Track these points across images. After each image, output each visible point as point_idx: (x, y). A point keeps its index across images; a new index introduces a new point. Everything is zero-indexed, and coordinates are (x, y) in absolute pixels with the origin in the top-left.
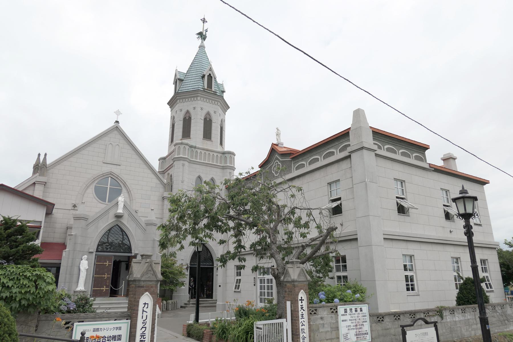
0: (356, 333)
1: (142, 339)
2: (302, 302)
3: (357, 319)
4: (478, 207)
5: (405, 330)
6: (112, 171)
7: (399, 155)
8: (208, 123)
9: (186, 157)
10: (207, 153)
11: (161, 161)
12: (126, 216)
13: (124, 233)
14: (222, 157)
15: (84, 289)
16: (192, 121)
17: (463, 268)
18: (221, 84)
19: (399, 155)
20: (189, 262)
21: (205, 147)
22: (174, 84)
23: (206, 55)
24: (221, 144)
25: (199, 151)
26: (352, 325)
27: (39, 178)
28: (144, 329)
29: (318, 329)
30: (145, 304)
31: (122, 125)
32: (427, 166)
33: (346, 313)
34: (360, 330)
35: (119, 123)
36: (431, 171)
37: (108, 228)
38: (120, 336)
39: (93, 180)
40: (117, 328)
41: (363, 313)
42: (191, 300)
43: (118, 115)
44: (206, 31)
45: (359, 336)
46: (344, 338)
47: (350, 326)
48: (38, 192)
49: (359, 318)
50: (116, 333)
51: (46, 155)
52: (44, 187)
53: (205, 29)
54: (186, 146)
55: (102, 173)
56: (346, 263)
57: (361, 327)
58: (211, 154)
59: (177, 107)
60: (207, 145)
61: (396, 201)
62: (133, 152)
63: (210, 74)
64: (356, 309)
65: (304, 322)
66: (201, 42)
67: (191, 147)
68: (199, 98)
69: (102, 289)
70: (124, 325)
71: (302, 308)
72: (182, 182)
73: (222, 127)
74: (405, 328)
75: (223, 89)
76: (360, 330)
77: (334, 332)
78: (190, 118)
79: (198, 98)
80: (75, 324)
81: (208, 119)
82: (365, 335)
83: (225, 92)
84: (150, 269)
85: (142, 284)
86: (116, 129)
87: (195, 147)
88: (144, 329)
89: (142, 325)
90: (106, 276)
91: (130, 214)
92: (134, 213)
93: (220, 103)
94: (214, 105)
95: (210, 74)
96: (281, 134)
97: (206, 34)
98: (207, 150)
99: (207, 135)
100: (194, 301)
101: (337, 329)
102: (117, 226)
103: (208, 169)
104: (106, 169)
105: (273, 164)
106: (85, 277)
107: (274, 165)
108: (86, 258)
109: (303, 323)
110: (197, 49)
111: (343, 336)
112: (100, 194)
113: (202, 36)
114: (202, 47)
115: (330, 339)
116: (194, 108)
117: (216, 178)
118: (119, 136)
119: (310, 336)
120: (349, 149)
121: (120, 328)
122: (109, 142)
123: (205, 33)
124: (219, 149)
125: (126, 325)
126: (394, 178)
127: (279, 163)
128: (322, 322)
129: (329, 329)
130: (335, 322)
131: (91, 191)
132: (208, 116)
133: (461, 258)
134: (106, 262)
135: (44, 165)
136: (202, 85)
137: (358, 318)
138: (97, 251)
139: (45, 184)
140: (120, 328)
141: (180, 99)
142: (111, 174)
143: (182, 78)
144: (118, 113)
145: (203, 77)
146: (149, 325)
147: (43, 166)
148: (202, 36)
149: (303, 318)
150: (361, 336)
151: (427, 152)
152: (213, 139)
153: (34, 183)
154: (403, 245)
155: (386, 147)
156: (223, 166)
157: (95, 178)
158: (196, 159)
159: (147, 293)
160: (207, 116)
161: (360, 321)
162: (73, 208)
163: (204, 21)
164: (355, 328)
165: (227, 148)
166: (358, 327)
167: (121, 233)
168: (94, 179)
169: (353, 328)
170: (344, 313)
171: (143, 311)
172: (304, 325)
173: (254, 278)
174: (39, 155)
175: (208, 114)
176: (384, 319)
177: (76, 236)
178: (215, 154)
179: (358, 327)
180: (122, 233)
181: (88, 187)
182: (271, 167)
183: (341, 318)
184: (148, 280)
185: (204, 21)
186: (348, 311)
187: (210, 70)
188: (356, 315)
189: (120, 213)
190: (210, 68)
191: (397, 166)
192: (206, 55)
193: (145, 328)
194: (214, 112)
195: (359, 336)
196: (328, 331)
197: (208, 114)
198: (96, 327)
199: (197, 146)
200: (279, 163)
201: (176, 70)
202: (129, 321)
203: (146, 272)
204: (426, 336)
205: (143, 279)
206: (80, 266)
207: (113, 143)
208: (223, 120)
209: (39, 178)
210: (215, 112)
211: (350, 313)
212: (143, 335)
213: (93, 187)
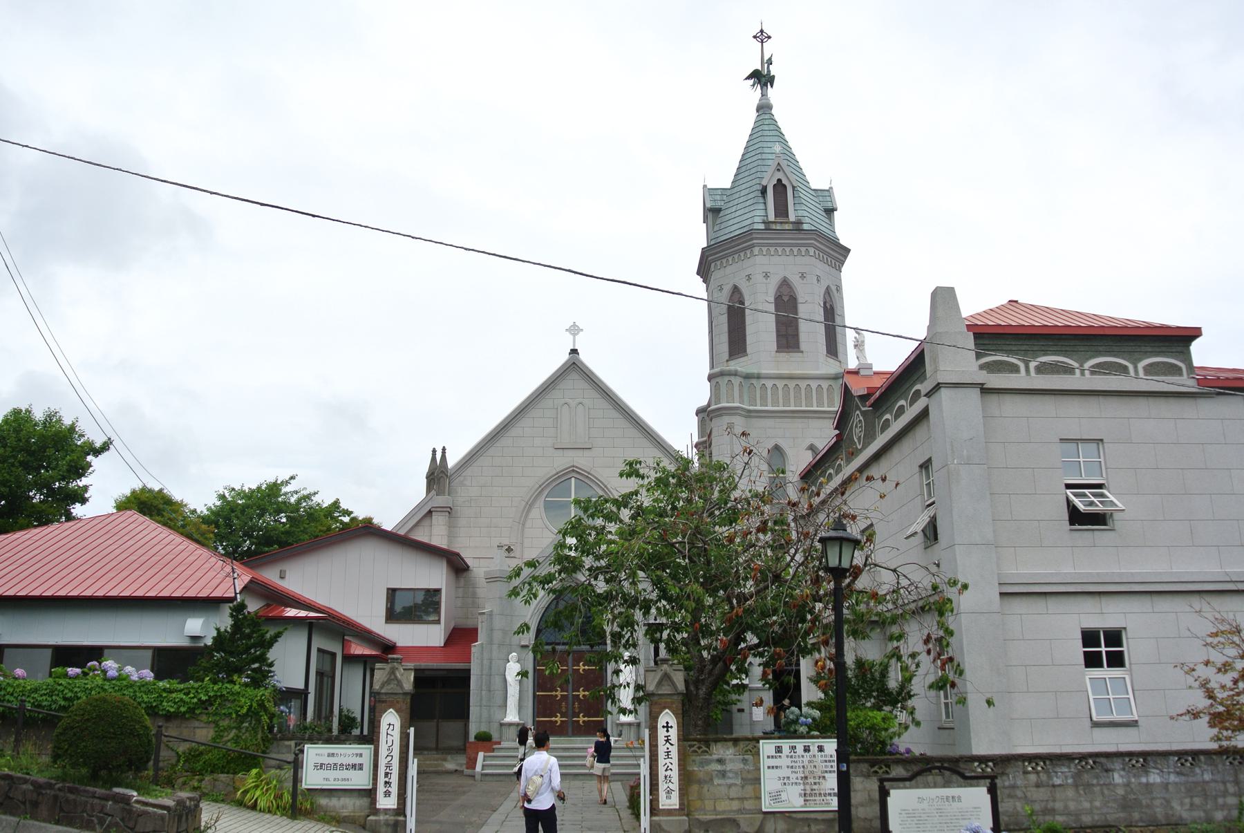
0: (803, 792)
1: (388, 771)
2: (668, 731)
3: (810, 767)
5: (884, 787)
6: (575, 464)
10: (792, 384)
11: (701, 415)
14: (833, 389)
15: (519, 719)
18: (828, 188)
21: (785, 371)
22: (704, 222)
25: (769, 384)
26: (794, 776)
27: (441, 501)
28: (389, 758)
29: (711, 780)
30: (390, 724)
31: (584, 357)
33: (778, 754)
35: (578, 354)
36: (1215, 396)
38: (361, 765)
39: (538, 488)
41: (826, 756)
43: (574, 335)
44: (770, 62)
45: (811, 798)
46: (772, 798)
47: (788, 778)
48: (437, 535)
49: (815, 764)
50: (357, 761)
51: (444, 449)
52: (449, 517)
53: (766, 58)
54: (732, 378)
55: (554, 472)
56: (1085, 652)
57: (817, 781)
58: (803, 384)
59: (716, 275)
60: (790, 364)
61: (1065, 496)
62: (614, 414)
63: (779, 181)
64: (807, 748)
65: (671, 764)
66: (760, 95)
67: (748, 377)
68: (756, 250)
69: (553, 719)
71: (667, 741)
73: (832, 308)
74: (885, 783)
77: (749, 788)
79: (753, 249)
81: (786, 299)
82: (828, 798)
83: (836, 210)
84: (393, 677)
85: (384, 697)
86: (574, 367)
87: (759, 377)
88: (389, 758)
89: (387, 753)
90: (559, 693)
93: (816, 248)
95: (779, 181)
96: (866, 342)
97: (769, 71)
98: (791, 377)
99: (788, 338)
101: (757, 780)
103: (799, 424)
104: (562, 461)
105: (853, 422)
106: (517, 696)
107: (855, 423)
108: (515, 659)
109: (668, 767)
110: (753, 115)
114: (764, 108)
115: (738, 799)
116: (749, 276)
118: (582, 384)
121: (361, 755)
122: (563, 401)
123: (768, 67)
125: (369, 751)
126: (1061, 439)
128: (719, 767)
129: (739, 782)
130: (754, 770)
132: (785, 290)
135: (442, 472)
137: (812, 765)
139: (449, 511)
141: (715, 260)
142: (573, 471)
143: (719, 204)
145: (764, 191)
147: (441, 475)
148: (762, 78)
149: (668, 758)
150: (816, 798)
151: (1196, 347)
152: (803, 346)
153: (430, 512)
154: (1089, 604)
157: (543, 484)
158: (752, 405)
160: (781, 290)
161: (815, 770)
164: (802, 782)
168: (540, 486)
169: (796, 783)
170: (774, 754)
171: (387, 734)
172: (671, 770)
174: (434, 451)
175: (785, 283)
176: (890, 769)
177: (491, 614)
178: (814, 384)
181: (530, 506)
183: (765, 762)
184: (390, 692)
187: (778, 170)
188: (806, 760)
190: (779, 164)
193: (391, 758)
194: (800, 275)
195: (811, 798)
197: (785, 283)
198: (331, 751)
199: (763, 372)
201: (705, 186)
203: (388, 682)
204: (956, 805)
205: (383, 691)
206: (507, 677)
207: (570, 401)
208: (833, 288)
209: (441, 501)
210: (803, 276)
211: (790, 755)
212: (388, 766)
213: (540, 503)
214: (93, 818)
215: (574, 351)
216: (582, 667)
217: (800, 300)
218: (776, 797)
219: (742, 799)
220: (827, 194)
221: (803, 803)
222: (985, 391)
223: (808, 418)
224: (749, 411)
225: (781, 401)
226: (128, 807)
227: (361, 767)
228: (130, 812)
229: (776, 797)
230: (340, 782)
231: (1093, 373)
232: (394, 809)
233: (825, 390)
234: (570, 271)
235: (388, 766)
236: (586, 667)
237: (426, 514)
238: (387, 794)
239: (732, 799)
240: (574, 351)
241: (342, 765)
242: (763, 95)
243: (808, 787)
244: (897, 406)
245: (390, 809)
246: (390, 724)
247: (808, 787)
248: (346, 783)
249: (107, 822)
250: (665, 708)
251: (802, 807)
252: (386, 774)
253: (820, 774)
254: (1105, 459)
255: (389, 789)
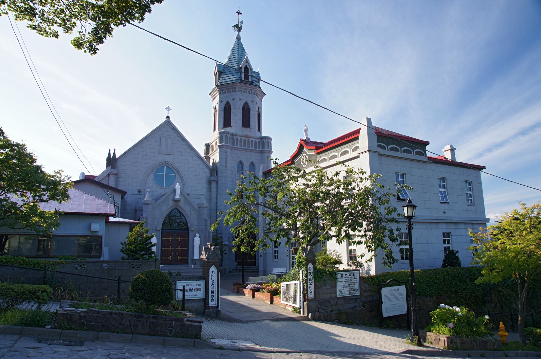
4: (473, 190)
7: (401, 152)
8: (246, 110)
9: (229, 145)
12: (182, 200)
13: (181, 214)
16: (232, 111)
17: (453, 241)
19: (401, 152)
20: (218, 141)
23: (241, 46)
24: (259, 129)
26: (346, 284)
27: (114, 171)
28: (213, 286)
30: (213, 272)
32: (426, 160)
34: (352, 288)
37: (169, 211)
40: (198, 285)
41: (355, 277)
42: (238, 267)
43: (168, 111)
44: (242, 23)
48: (112, 184)
50: (199, 287)
51: (115, 150)
54: (227, 135)
55: (159, 163)
63: (246, 66)
70: (202, 283)
72: (226, 167)
75: (259, 77)
76: (352, 288)
78: (230, 108)
80: (177, 282)
87: (236, 135)
88: (213, 286)
91: (186, 200)
92: (186, 196)
94: (251, 95)
95: (246, 66)
97: (241, 26)
98: (247, 137)
99: (246, 123)
100: (240, 267)
102: (176, 209)
107: (302, 158)
111: (339, 291)
112: (158, 179)
113: (238, 28)
114: (238, 39)
115: (330, 293)
117: (254, 162)
119: (315, 291)
120: (358, 151)
121: (200, 285)
123: (241, 25)
124: (257, 134)
125: (203, 283)
127: (307, 156)
129: (330, 287)
131: (151, 178)
133: (452, 233)
134: (170, 238)
136: (239, 76)
138: (162, 229)
140: (200, 285)
144: (168, 109)
146: (215, 283)
148: (238, 28)
151: (428, 148)
152: (251, 126)
155: (389, 147)
156: (261, 151)
159: (213, 266)
162: (139, 193)
163: (239, 13)
165: (264, 134)
166: (351, 286)
167: (179, 214)
171: (212, 276)
173: (288, 250)
174: (110, 150)
179: (351, 286)
180: (180, 215)
182: (300, 159)
185: (239, 13)
186: (344, 276)
187: (246, 62)
188: (349, 278)
189: (177, 198)
191: (399, 162)
192: (241, 46)
196: (329, 288)
200: (307, 156)
202: (204, 281)
204: (398, 291)
208: (260, 107)
210: (252, 102)
212: (213, 289)
214: (166, 330)
215: (168, 117)
216: (179, 239)
217: (251, 110)
218: (341, 292)
219: (331, 293)
220: (257, 73)
221: (348, 293)
222: (380, 155)
223: (251, 152)
224: (232, 147)
225: (254, 146)
226: (183, 323)
227: (200, 290)
228: (184, 325)
229: (341, 292)
230: (192, 297)
231: (416, 154)
232: (216, 306)
233: (250, 142)
234: (290, 93)
235: (213, 289)
236: (181, 239)
237: (107, 175)
238: (212, 300)
239: (328, 294)
240: (168, 117)
241: (192, 289)
242: (238, 34)
243: (350, 288)
244: (330, 156)
245: (214, 306)
246: (213, 272)
247: (350, 288)
248: (194, 296)
249: (173, 332)
250: (309, 262)
251: (348, 295)
252: (212, 292)
253: (353, 283)
254: (446, 183)
255: (213, 298)
